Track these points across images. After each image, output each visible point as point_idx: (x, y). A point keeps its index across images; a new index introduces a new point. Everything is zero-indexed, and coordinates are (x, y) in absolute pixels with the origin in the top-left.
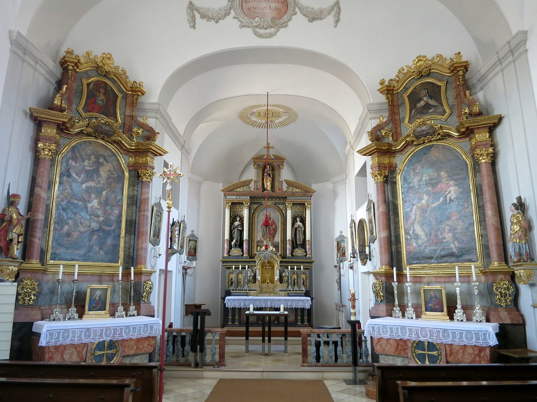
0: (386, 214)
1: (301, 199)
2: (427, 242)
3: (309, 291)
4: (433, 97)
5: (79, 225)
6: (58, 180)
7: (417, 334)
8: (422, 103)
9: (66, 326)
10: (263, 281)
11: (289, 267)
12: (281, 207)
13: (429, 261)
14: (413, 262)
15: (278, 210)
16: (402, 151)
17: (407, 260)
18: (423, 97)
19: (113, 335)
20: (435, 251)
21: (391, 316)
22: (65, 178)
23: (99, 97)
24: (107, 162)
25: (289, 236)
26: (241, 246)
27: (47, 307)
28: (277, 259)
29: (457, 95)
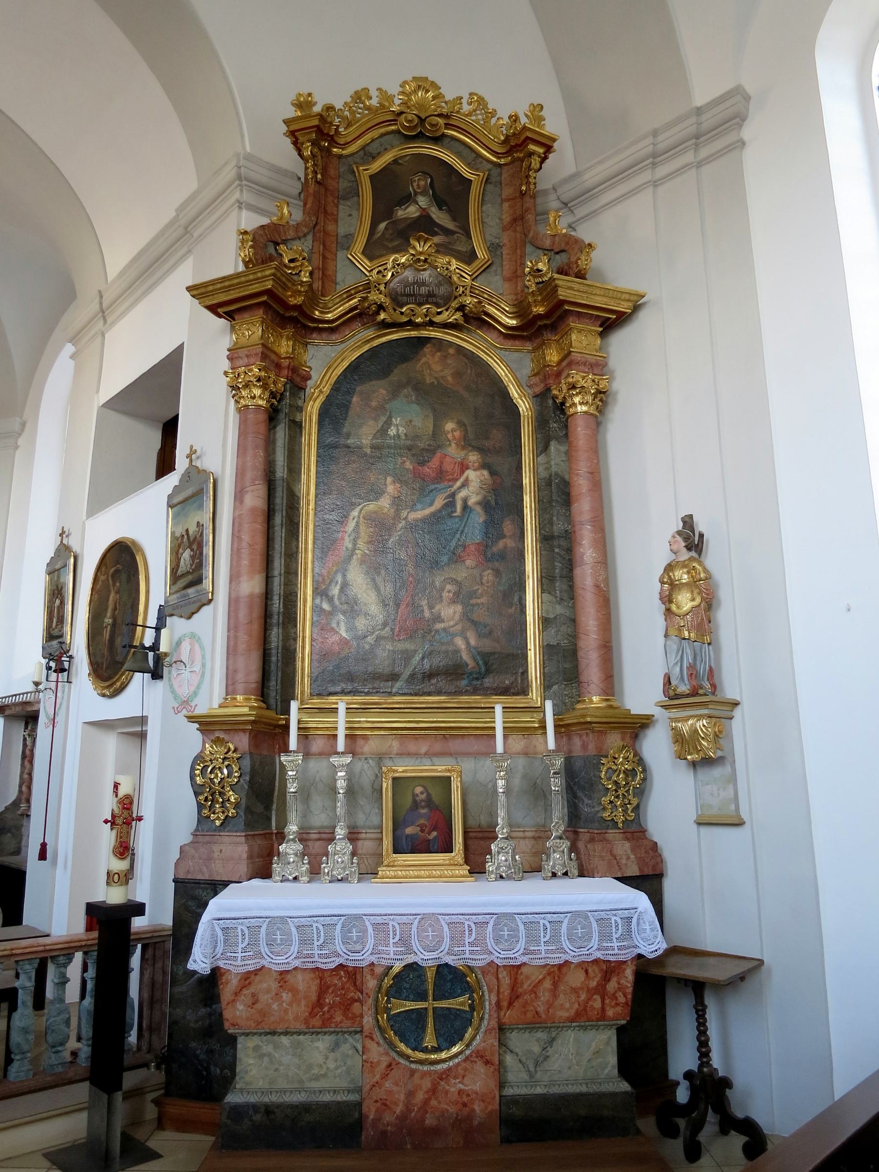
0: (261, 519)
2: (385, 625)
4: (447, 205)
7: (404, 941)
8: (411, 211)
13: (386, 686)
14: (332, 689)
16: (332, 330)
17: (314, 680)
18: (416, 193)
20: (407, 656)
21: (265, 873)
29: (515, 220)
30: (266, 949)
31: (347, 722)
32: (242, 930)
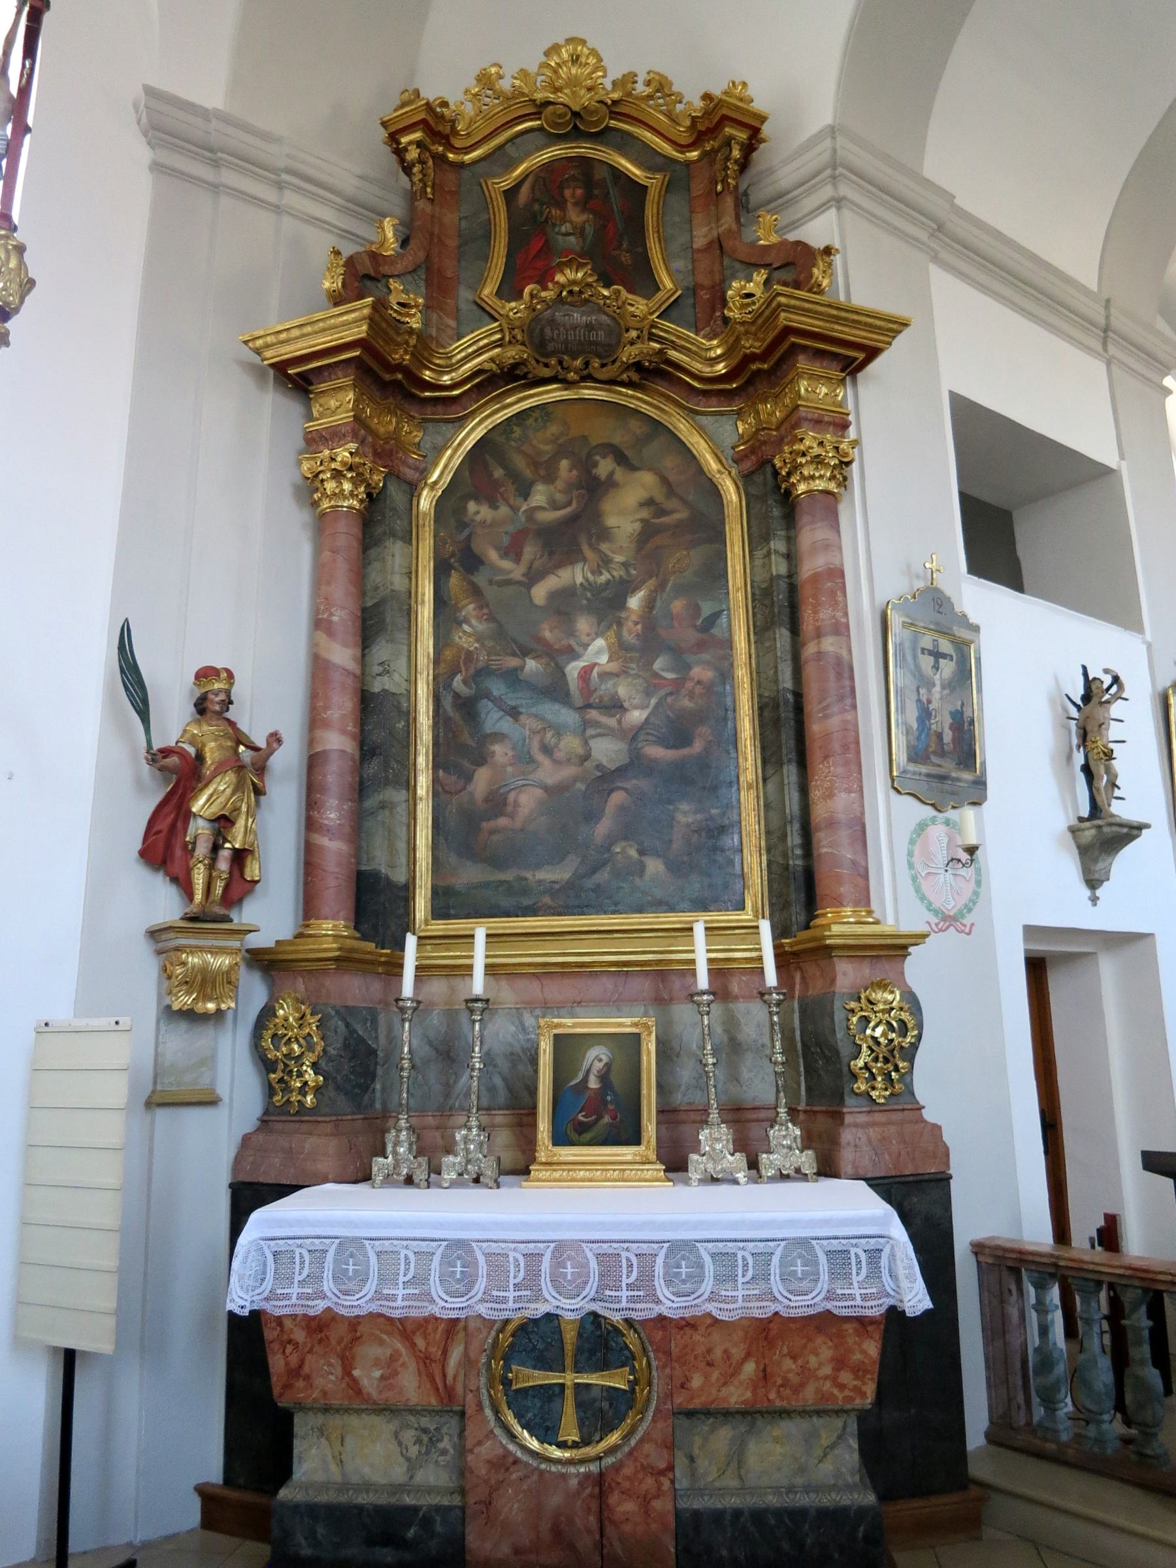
5: (540, 757)
6: (427, 590)
9: (350, 1224)
19: (601, 1288)
22: (455, 580)
23: (564, 220)
24: (632, 468)
27: (430, 1121)
30: (332, 1285)
31: (693, 951)
32: (857, 1255)
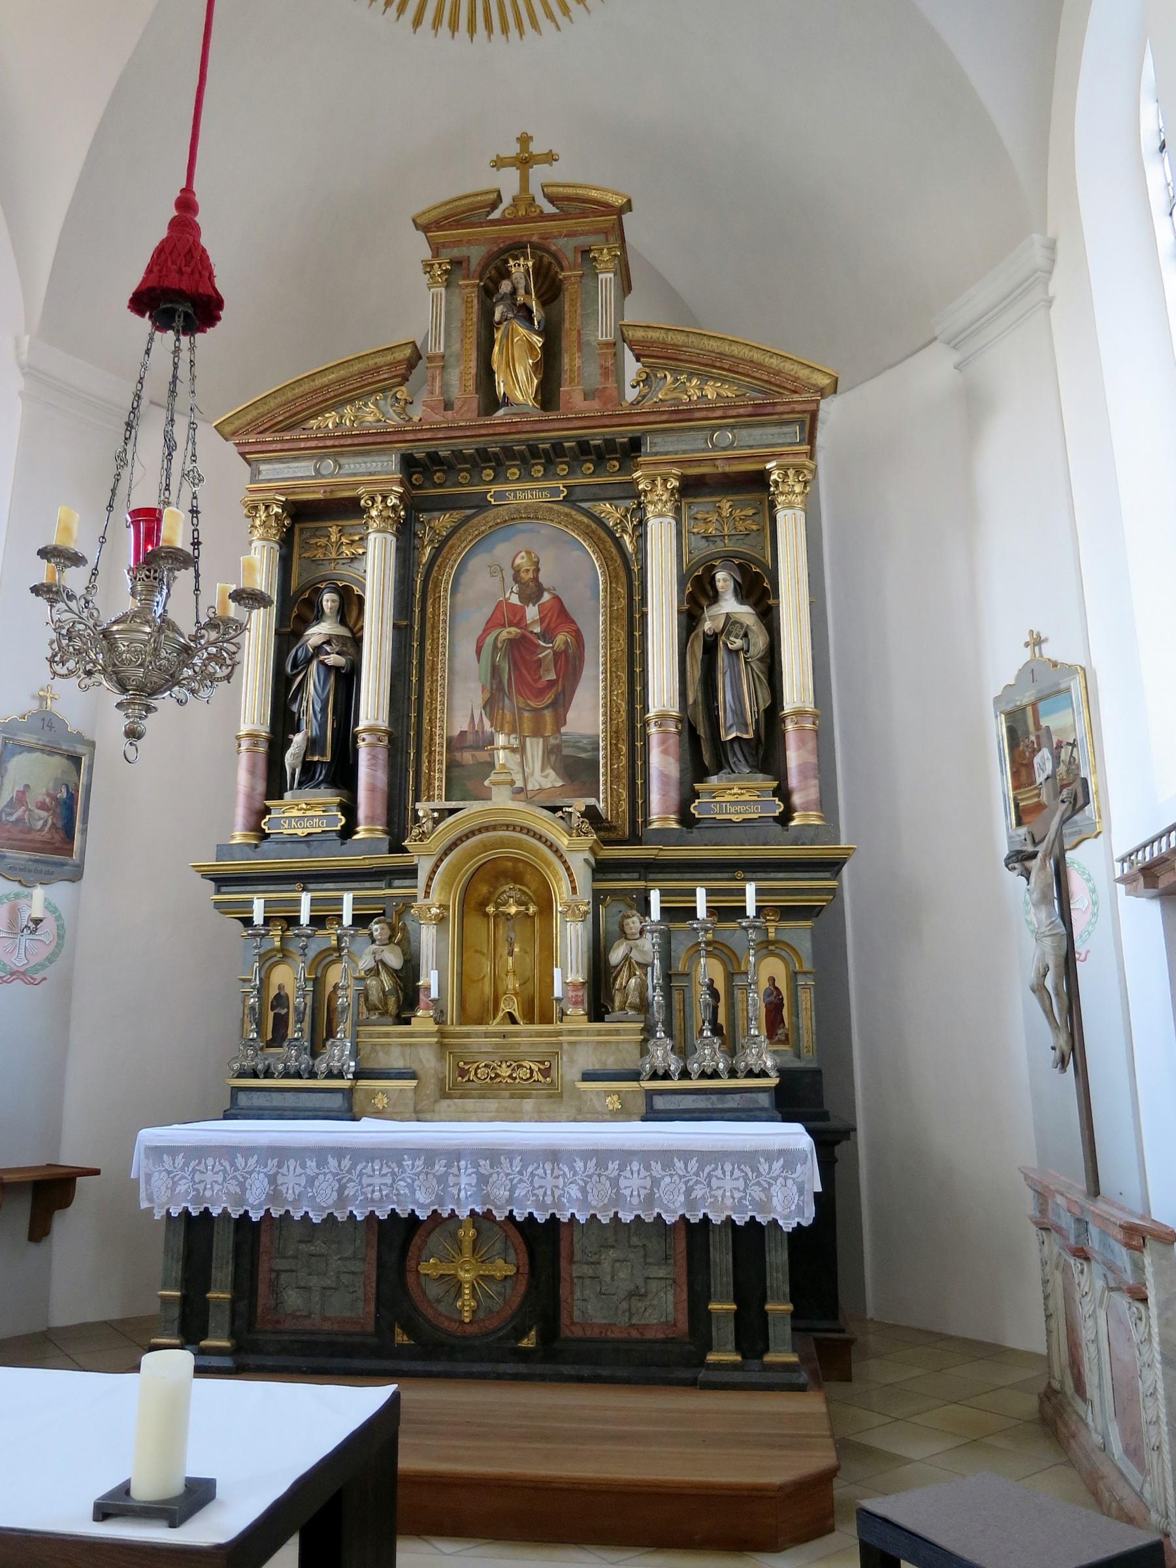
1: (740, 457)
3: (816, 1074)
10: (476, 1009)
11: (655, 897)
12: (609, 512)
15: (588, 534)
25: (663, 690)
26: (341, 774)
28: (563, 841)
